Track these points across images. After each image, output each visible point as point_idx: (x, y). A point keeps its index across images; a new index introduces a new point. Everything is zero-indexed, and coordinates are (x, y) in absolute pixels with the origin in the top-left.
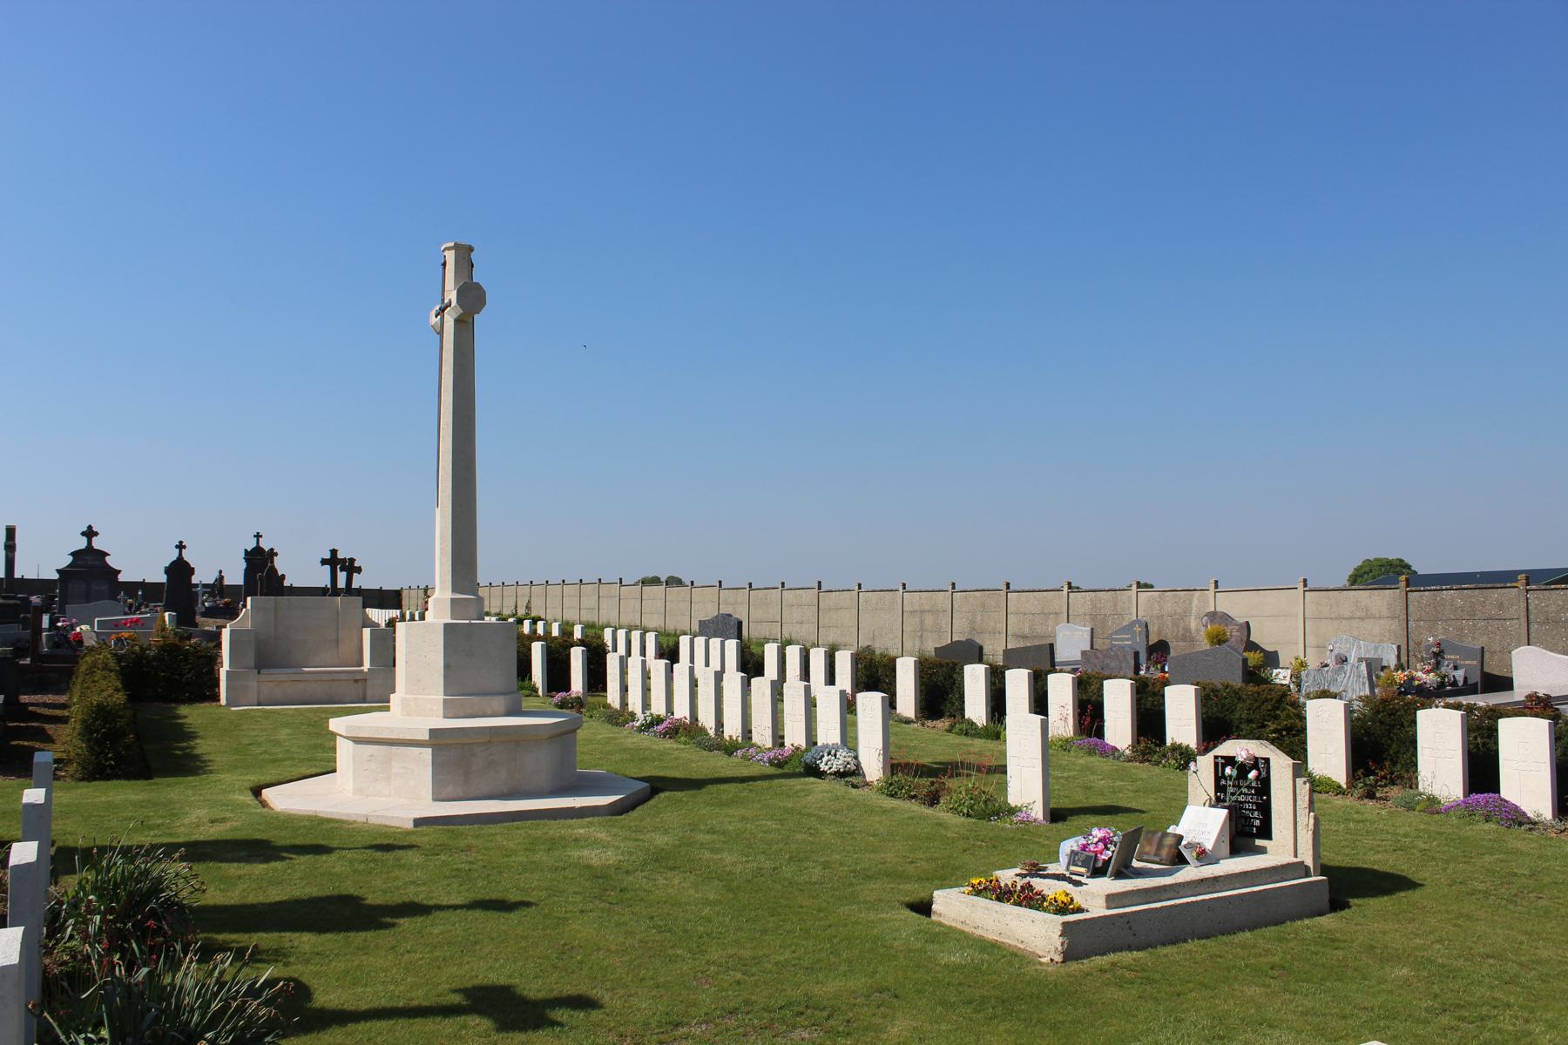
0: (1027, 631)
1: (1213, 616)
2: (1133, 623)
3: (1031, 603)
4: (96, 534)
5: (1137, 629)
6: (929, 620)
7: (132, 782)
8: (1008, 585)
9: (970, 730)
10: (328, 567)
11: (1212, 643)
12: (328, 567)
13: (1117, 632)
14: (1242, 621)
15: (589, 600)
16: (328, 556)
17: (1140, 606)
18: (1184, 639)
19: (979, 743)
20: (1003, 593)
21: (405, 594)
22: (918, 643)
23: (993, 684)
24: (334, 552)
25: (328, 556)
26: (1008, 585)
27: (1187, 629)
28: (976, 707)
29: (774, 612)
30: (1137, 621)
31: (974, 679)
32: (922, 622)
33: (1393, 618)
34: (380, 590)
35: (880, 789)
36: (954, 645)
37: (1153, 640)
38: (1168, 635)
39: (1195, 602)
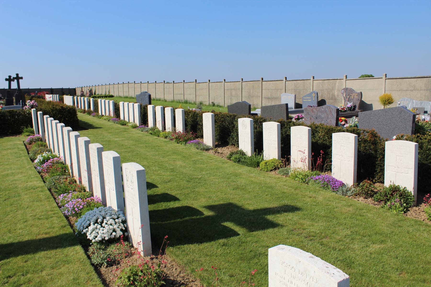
0: (269, 96)
1: (346, 89)
2: (312, 93)
3: (271, 85)
4: (10, 77)
5: (313, 95)
6: (234, 93)
7: (86, 121)
8: (262, 79)
9: (240, 158)
10: (8, 82)
11: (385, 104)
12: (8, 82)
13: (305, 96)
14: (359, 91)
15: (126, 89)
16: (8, 78)
17: (315, 86)
18: (332, 99)
19: (244, 169)
20: (261, 82)
21: (77, 89)
22: (230, 101)
23: (255, 128)
24: (22, 78)
25: (8, 78)
26: (262, 79)
27: (333, 95)
28: (245, 144)
29: (181, 91)
30: (313, 92)
31: (244, 126)
32: (231, 93)
33: (427, 90)
34: (69, 89)
35: (217, 146)
36: (237, 105)
37: (320, 99)
38: (325, 98)
39: (337, 84)
